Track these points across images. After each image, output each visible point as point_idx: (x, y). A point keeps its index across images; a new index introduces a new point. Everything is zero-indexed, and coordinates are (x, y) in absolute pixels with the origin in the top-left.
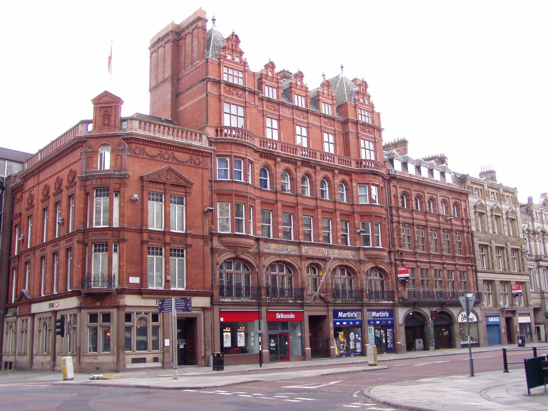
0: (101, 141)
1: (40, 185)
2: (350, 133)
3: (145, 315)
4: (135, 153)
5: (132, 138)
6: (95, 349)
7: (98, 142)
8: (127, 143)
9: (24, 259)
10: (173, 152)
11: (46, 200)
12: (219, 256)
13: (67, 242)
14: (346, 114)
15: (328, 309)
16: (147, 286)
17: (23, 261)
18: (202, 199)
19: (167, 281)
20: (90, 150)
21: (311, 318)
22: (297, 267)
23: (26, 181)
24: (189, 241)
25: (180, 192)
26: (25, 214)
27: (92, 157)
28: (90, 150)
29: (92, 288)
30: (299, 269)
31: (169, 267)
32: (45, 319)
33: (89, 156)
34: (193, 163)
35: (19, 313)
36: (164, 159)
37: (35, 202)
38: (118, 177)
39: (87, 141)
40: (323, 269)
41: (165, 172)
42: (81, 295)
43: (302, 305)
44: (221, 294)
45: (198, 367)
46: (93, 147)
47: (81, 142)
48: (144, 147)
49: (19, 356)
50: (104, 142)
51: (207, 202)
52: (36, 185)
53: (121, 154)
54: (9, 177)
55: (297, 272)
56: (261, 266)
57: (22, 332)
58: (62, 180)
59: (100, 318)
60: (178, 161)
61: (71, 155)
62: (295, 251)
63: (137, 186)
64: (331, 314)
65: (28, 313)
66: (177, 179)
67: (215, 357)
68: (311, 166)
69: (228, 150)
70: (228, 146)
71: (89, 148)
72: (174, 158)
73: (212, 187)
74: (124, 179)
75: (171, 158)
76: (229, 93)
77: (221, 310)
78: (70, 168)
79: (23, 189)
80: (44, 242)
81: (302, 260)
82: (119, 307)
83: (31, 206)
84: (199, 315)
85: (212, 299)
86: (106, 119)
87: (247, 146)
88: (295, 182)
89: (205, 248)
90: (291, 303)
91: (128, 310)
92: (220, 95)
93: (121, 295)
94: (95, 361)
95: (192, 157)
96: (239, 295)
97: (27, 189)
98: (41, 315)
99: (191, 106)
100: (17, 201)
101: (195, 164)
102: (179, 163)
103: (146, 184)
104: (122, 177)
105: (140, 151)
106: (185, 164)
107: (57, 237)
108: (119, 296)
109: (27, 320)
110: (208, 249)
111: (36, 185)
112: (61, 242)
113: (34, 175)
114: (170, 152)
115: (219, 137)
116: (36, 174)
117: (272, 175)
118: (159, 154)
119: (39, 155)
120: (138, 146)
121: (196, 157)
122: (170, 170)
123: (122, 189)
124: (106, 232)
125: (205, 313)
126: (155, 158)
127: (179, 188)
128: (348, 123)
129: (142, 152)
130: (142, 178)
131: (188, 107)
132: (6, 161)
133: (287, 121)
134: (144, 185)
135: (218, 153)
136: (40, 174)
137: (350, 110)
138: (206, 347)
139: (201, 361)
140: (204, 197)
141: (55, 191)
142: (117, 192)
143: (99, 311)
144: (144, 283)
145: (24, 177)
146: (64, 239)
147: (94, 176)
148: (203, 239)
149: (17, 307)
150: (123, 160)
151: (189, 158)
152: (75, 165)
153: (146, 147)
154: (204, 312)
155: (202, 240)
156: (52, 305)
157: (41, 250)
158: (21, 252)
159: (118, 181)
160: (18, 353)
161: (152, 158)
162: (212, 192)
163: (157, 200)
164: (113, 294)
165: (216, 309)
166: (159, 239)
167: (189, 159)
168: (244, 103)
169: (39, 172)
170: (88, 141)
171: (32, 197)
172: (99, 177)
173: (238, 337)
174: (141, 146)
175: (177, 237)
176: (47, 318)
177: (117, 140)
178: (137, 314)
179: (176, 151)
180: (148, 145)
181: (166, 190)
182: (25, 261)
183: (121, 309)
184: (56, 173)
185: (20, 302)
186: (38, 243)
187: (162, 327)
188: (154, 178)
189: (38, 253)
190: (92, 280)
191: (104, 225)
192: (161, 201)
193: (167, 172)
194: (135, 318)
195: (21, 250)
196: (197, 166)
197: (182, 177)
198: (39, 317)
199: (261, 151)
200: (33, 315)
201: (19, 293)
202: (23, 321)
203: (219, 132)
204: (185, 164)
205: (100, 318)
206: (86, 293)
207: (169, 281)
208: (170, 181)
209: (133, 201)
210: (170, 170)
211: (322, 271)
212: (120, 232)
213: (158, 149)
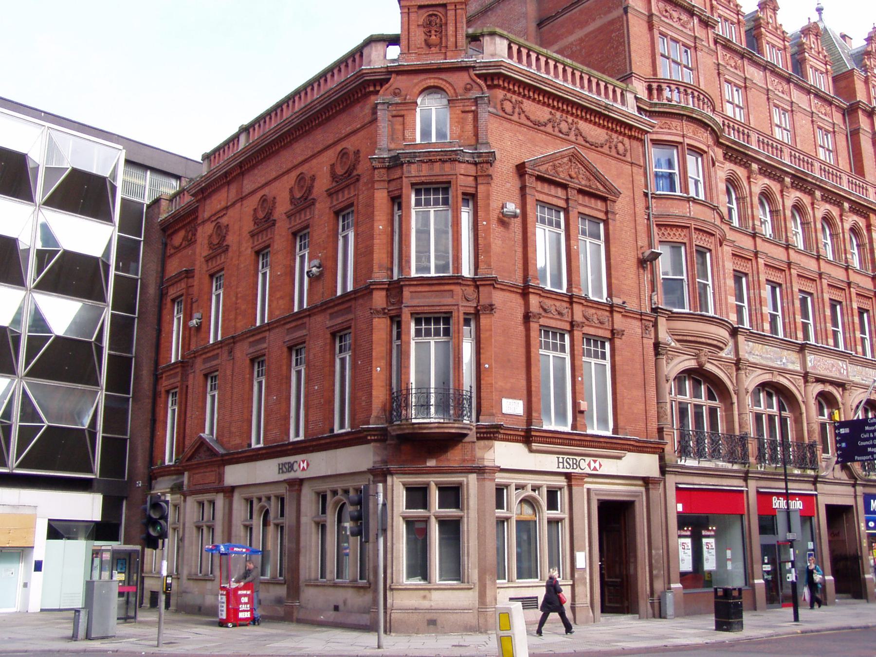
0: (425, 79)
1: (244, 202)
2: (861, 131)
3: (532, 493)
4: (504, 111)
5: (500, 75)
6: (424, 574)
7: (415, 81)
8: (489, 87)
9: (200, 366)
10: (576, 120)
11: (266, 229)
12: (668, 363)
13: (252, 344)
14: (853, 93)
15: (855, 492)
16: (541, 423)
17: (198, 371)
18: (633, 231)
19: (578, 412)
20: (397, 100)
21: (830, 508)
22: (800, 398)
23: (205, 199)
24: (619, 321)
25: (596, 208)
26: (201, 268)
27: (403, 116)
28: (397, 100)
29: (414, 421)
30: (803, 402)
31: (582, 379)
32: (264, 499)
33: (394, 113)
34: (613, 150)
35: (189, 486)
36: (560, 131)
37: (231, 239)
38: (471, 159)
39: (390, 79)
40: (841, 406)
41: (565, 160)
42: (385, 440)
43: (815, 481)
44: (684, 451)
45: (640, 618)
46: (403, 93)
47: (375, 83)
48: (520, 99)
49: (191, 582)
50: (431, 82)
51: (643, 241)
52: (234, 204)
53: (473, 108)
54: (157, 202)
55: (183, 477)
56: (742, 392)
57: (199, 528)
58: (313, 178)
59: (434, 496)
60: (587, 142)
61: (344, 117)
62: (793, 363)
63: (513, 184)
64: (860, 501)
65: (215, 485)
66: (590, 180)
67: (720, 597)
68: (806, 188)
69: (675, 131)
70: (675, 123)
71: (395, 94)
72: (579, 133)
73: (648, 208)
74: (485, 165)
75: (573, 133)
76: (664, 13)
77: (680, 486)
78: (339, 148)
79: (197, 217)
80: (266, 322)
81: (806, 381)
82: (481, 471)
83: (219, 247)
84: (637, 496)
85: (662, 459)
86: (433, 32)
87: (709, 126)
88: (782, 218)
89: (645, 340)
90: (797, 475)
91: (501, 478)
92: (651, 16)
93: (487, 442)
94: (426, 604)
95: (611, 137)
96: (715, 454)
97: (207, 215)
98: (252, 489)
99: (581, 40)
100: (172, 251)
101: (618, 154)
102: (588, 145)
103: (530, 182)
104: (481, 159)
105: (514, 108)
106: (599, 149)
107: (305, 307)
108: (482, 443)
109: (212, 503)
110: (649, 343)
111: (234, 204)
112: (313, 319)
113: (228, 183)
114: (570, 119)
115: (655, 101)
116: (235, 178)
117: (744, 198)
118: (549, 121)
119: (243, 138)
120: (509, 95)
121: (617, 138)
122: (574, 157)
123: (481, 188)
124: (447, 288)
125: (651, 491)
126: (542, 128)
127: (593, 201)
128: (857, 112)
129: (517, 110)
130: (521, 169)
131: (572, 44)
132: (149, 173)
133: (758, 93)
134: (527, 184)
135: (655, 137)
136: (246, 177)
137: (859, 86)
138: (655, 572)
139: (644, 604)
140: (638, 228)
141: (290, 207)
142: (470, 197)
143: (433, 480)
144: (534, 414)
145: (202, 191)
146: (244, 339)
147: (414, 155)
148: (641, 320)
149: (183, 474)
150: (481, 122)
151: (607, 137)
152: (353, 139)
153: (525, 100)
154: (647, 490)
155: (638, 323)
156: (291, 467)
157: (331, 314)
158: (195, 352)
159: (472, 170)
160: (190, 574)
161: (537, 125)
162: (648, 219)
163: (550, 223)
164: (467, 439)
165: (671, 481)
166: (560, 313)
167: (607, 141)
168: (693, 40)
169: (243, 174)
170: (391, 80)
171: (221, 231)
172: (425, 159)
173: (705, 548)
174: (515, 98)
175: (594, 311)
176: (269, 498)
177: (460, 80)
178: (516, 489)
179: (582, 118)
180: (529, 98)
181: (570, 202)
182: (204, 372)
183: (486, 476)
184: (295, 167)
185: (194, 462)
186: (241, 326)
187: (567, 521)
188: (545, 170)
189: (243, 351)
190: (413, 400)
191: (437, 271)
192: (558, 225)
193: (570, 160)
194: (513, 497)
195: (193, 348)
196: (620, 157)
197: (596, 176)
198: (247, 495)
199: (727, 143)
200: (230, 491)
201: (188, 442)
202: (201, 504)
203: (655, 92)
204: (599, 149)
205: (434, 496)
206: (399, 436)
207: (582, 412)
208: (577, 181)
209: (504, 221)
210: (574, 157)
211: (839, 409)
212: (481, 289)
213: (547, 110)
